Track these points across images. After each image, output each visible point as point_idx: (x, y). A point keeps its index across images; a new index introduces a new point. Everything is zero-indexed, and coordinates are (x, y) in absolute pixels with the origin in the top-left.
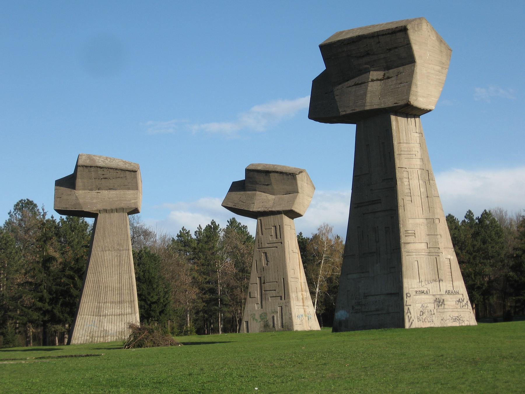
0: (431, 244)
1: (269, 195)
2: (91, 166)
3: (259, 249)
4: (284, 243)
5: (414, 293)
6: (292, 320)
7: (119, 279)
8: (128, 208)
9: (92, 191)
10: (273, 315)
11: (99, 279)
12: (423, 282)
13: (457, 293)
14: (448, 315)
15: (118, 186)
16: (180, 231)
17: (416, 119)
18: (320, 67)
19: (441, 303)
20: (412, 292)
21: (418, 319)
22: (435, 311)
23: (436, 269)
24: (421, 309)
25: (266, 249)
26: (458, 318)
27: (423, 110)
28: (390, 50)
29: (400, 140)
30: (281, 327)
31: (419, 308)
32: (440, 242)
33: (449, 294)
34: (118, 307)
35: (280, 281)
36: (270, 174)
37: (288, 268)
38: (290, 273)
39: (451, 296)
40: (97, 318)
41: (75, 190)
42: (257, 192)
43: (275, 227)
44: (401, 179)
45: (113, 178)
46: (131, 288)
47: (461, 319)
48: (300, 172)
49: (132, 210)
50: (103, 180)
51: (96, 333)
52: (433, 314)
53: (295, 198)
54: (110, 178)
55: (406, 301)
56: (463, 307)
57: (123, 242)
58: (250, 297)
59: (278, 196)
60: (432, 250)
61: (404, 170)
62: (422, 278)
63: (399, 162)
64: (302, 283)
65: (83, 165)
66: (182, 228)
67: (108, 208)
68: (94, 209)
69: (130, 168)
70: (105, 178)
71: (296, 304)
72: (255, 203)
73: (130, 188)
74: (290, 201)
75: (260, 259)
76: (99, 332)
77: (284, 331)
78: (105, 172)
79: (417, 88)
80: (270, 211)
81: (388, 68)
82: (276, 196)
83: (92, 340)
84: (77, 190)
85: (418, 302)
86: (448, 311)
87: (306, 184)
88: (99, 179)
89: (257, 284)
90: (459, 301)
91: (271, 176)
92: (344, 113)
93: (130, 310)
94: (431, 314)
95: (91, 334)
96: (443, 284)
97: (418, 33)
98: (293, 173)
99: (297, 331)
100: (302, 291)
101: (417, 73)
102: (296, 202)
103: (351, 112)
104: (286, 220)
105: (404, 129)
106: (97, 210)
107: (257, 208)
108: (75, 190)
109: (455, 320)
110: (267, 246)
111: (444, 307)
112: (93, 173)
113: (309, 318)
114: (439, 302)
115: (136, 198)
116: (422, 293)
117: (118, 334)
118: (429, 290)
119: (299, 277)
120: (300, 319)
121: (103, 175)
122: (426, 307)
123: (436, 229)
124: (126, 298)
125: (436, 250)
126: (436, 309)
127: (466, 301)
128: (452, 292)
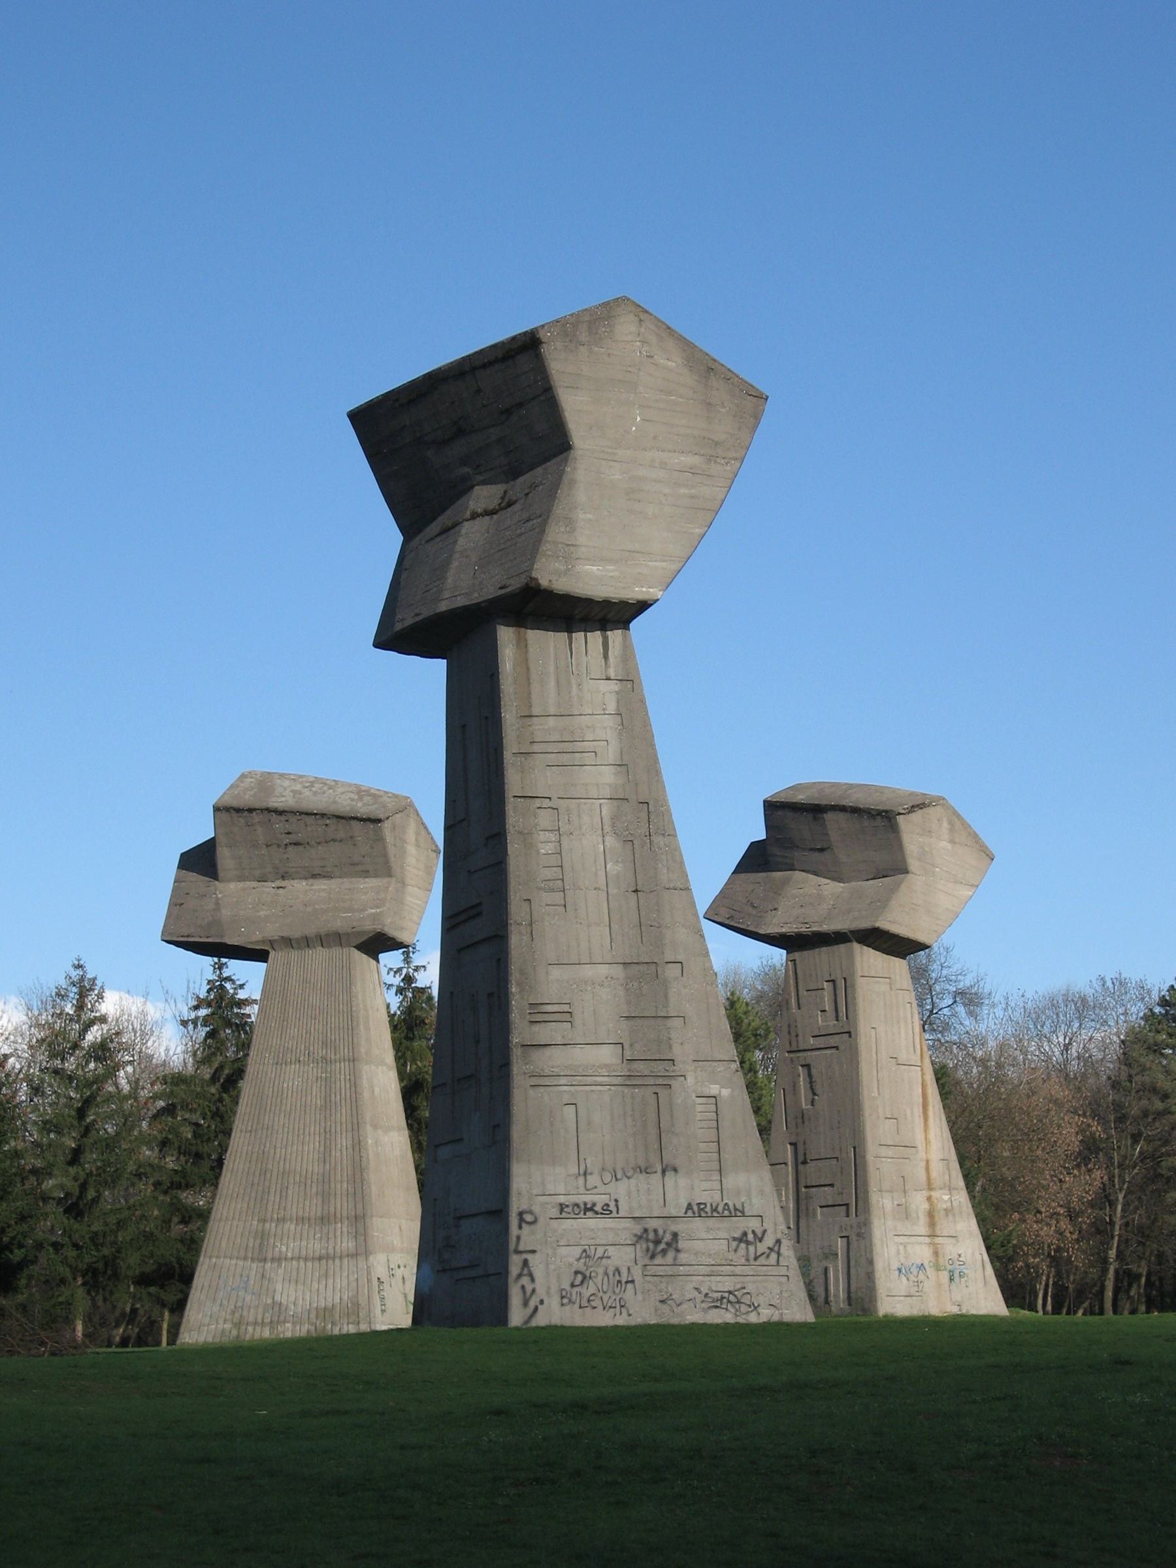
1: (829, 881)
2: (252, 807)
3: (792, 1055)
4: (857, 1035)
5: (555, 1212)
6: (874, 1282)
8: (353, 932)
9: (263, 883)
10: (825, 1263)
11: (266, 1149)
12: (591, 1174)
13: (739, 1212)
14: (690, 1286)
15: (336, 866)
17: (609, 633)
19: (662, 1246)
20: (544, 1207)
21: (562, 1297)
22: (637, 1273)
23: (653, 1132)
24: (580, 1266)
25: (809, 1053)
26: (732, 1298)
27: (607, 604)
28: (508, 412)
29: (531, 706)
30: (846, 1303)
31: (571, 1260)
32: (680, 1041)
33: (700, 1216)
36: (825, 815)
39: (711, 1222)
40: (254, 1266)
41: (217, 880)
42: (797, 872)
44: (526, 836)
45: (319, 843)
46: (358, 1176)
47: (746, 1299)
48: (913, 807)
49: (366, 937)
50: (290, 848)
51: (252, 1310)
52: (627, 1282)
53: (893, 890)
54: (308, 843)
55: (518, 1238)
56: (756, 1259)
59: (854, 883)
60: (641, 1067)
65: (228, 806)
67: (296, 934)
68: (254, 939)
72: (780, 908)
73: (368, 871)
74: (879, 901)
75: (794, 1086)
76: (260, 1310)
79: (573, 530)
81: (513, 473)
82: (847, 884)
83: (239, 1332)
84: (222, 881)
85: (568, 1241)
86: (691, 1273)
87: (945, 844)
89: (785, 1164)
90: (742, 1239)
91: (827, 823)
93: (352, 1245)
94: (619, 1282)
95: (237, 1315)
96: (676, 1182)
98: (886, 812)
100: (930, 1188)
101: (572, 482)
102: (893, 903)
104: (869, 960)
105: (552, 669)
106: (263, 942)
107: (779, 924)
108: (217, 882)
109: (719, 1302)
110: (812, 1045)
111: (675, 1259)
112: (260, 830)
113: (956, 1275)
114: (657, 1242)
116: (586, 1210)
117: (313, 1315)
118: (616, 1201)
120: (912, 1278)
121: (289, 833)
122: (602, 1258)
125: (659, 1068)
126: (640, 1266)
127: (774, 1241)
128: (715, 1210)
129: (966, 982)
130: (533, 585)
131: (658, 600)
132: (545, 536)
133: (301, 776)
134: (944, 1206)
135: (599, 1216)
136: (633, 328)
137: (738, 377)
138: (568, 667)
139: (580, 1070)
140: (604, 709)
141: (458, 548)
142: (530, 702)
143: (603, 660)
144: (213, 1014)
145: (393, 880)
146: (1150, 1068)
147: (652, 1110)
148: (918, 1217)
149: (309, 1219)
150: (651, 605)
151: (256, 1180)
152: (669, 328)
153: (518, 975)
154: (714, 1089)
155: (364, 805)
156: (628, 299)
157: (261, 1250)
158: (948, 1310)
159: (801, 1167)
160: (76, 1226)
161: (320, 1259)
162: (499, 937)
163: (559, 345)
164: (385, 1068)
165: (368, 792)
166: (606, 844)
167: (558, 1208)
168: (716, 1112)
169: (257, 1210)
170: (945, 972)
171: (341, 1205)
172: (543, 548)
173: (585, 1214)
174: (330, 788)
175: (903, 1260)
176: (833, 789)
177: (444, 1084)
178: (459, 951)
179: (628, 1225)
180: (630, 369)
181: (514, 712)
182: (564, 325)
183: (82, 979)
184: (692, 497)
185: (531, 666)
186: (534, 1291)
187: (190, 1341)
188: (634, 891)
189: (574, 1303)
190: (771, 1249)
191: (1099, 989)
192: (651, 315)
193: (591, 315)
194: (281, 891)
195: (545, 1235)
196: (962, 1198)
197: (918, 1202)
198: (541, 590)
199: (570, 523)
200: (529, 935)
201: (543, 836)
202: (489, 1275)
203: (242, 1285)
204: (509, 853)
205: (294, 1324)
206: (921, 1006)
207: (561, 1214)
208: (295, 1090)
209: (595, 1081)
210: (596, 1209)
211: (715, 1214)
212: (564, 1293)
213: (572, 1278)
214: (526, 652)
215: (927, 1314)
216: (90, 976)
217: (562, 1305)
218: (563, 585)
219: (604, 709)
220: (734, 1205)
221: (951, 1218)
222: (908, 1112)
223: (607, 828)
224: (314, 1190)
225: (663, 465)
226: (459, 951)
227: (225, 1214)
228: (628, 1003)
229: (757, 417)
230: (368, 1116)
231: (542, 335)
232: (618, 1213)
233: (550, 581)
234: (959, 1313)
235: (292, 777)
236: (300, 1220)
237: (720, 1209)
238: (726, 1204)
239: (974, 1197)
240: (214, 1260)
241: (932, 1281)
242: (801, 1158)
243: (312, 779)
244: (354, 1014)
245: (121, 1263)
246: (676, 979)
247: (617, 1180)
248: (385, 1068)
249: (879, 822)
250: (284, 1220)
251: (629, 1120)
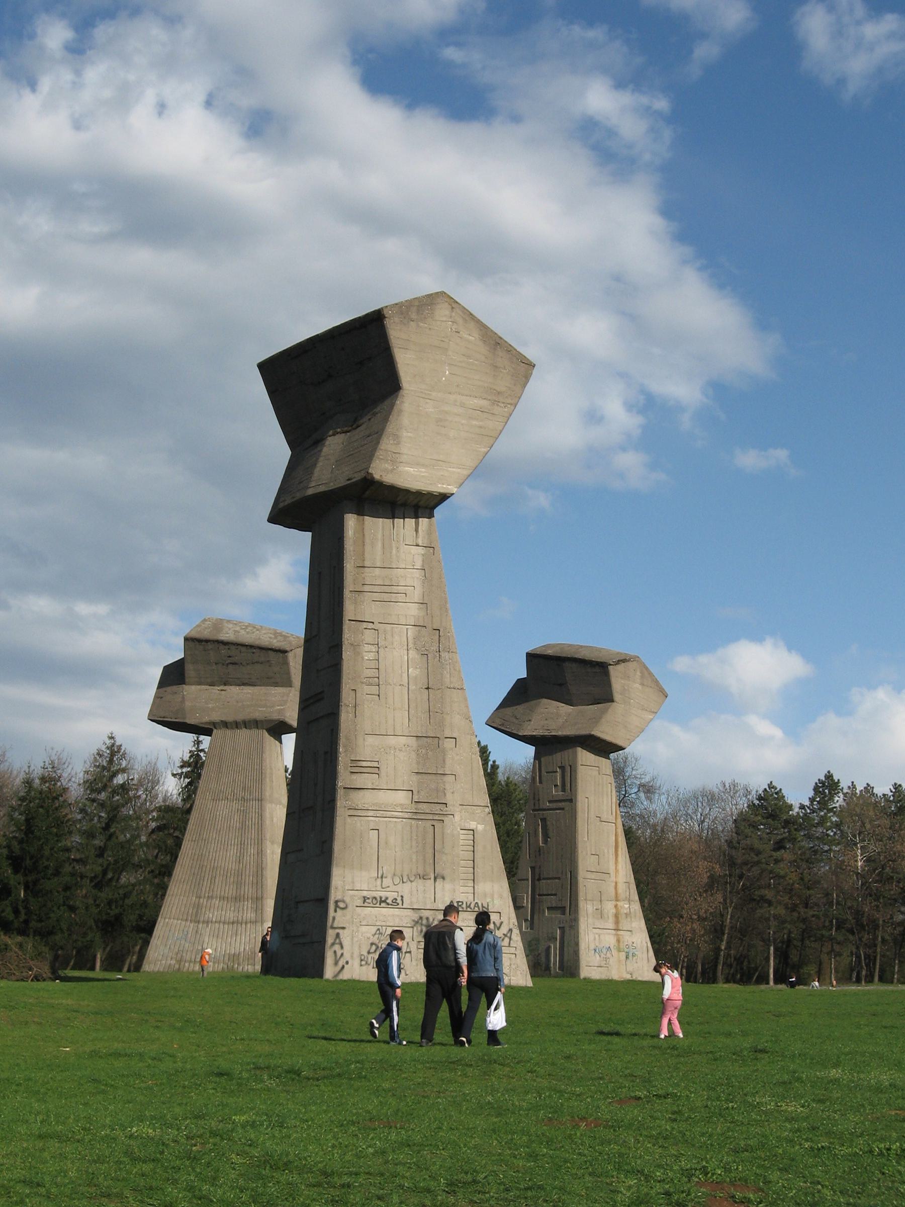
0: (422, 793)
5: (359, 902)
6: (578, 957)
7: (238, 854)
11: (204, 853)
12: (386, 877)
16: (765, 789)
20: (353, 899)
23: (431, 851)
29: (364, 560)
31: (369, 935)
32: (451, 791)
34: (232, 908)
38: (586, 862)
40: (192, 925)
44: (355, 646)
48: (618, 661)
50: (230, 666)
51: (188, 953)
52: (406, 953)
55: (334, 918)
57: (252, 784)
61: (365, 627)
62: (387, 869)
63: (355, 608)
64: (618, 884)
66: (768, 784)
67: (230, 718)
70: (233, 664)
71: (594, 925)
72: (533, 720)
74: (594, 718)
76: (194, 954)
77: (563, 976)
79: (399, 443)
85: (368, 922)
87: (637, 685)
88: (223, 664)
93: (253, 915)
95: (179, 955)
97: (418, 325)
99: (587, 981)
101: (400, 411)
104: (584, 757)
105: (380, 536)
106: (209, 723)
113: (630, 955)
116: (381, 902)
117: (226, 958)
118: (402, 897)
120: (602, 955)
121: (230, 657)
123: (444, 761)
124: (249, 891)
125: (437, 808)
126: (415, 941)
127: (508, 929)
129: (646, 779)
130: (369, 478)
131: (453, 494)
132: (379, 446)
133: (240, 622)
134: (625, 912)
135: (390, 906)
136: (447, 312)
137: (516, 350)
138: (391, 535)
139: (383, 806)
140: (413, 566)
141: (323, 454)
142: (363, 557)
143: (415, 533)
144: (193, 771)
145: (293, 688)
146: (751, 837)
147: (431, 836)
148: (608, 917)
149: (227, 898)
150: (449, 497)
151: (196, 873)
152: (471, 314)
153: (344, 740)
154: (473, 825)
155: (278, 641)
156: (445, 293)
157: (196, 915)
158: (624, 977)
159: (537, 883)
160: (99, 894)
161: (233, 923)
162: (333, 715)
163: (396, 319)
164: (281, 806)
165: (281, 634)
166: (410, 655)
167: (363, 899)
168: (473, 841)
169: (195, 891)
170: (634, 772)
171: (249, 891)
172: (377, 454)
173: (380, 904)
174: (258, 630)
175: (597, 944)
176: (570, 648)
177: (294, 812)
178: (309, 723)
179: (409, 914)
180: (443, 339)
181: (352, 563)
182: (401, 307)
183: (113, 745)
184: (481, 427)
185: (366, 533)
186: (342, 954)
187: (149, 970)
188: (426, 688)
189: (369, 965)
190: (505, 935)
191: (722, 789)
192: (460, 304)
193: (420, 302)
194: (223, 692)
195: (352, 917)
196: (636, 907)
197: (609, 908)
198: (375, 482)
199: (397, 437)
200: (354, 714)
201: (367, 648)
202: (313, 943)
203: (184, 937)
204: (343, 657)
205: (214, 963)
206: (619, 791)
207: (364, 903)
208: (224, 816)
209: (386, 814)
210: (388, 901)
211: (469, 909)
212: (363, 958)
213: (369, 947)
214: (363, 524)
215: (610, 978)
216: (118, 743)
217: (361, 965)
218: (389, 479)
219: (413, 566)
220: (482, 904)
221: (629, 919)
222: (606, 851)
223: (411, 645)
224: (232, 880)
225: (462, 405)
226: (309, 723)
227: (175, 893)
228: (418, 763)
229: (527, 377)
230: (268, 836)
231: (385, 312)
232: (402, 905)
233: (381, 476)
234: (631, 979)
235: (235, 622)
236: (222, 898)
237: (472, 906)
238: (477, 903)
239: (644, 906)
240: (167, 920)
241: (616, 958)
242: (537, 877)
243: (246, 624)
244: (263, 771)
245: (125, 917)
246: (452, 749)
247: (403, 882)
248: (281, 806)
249: (597, 670)
250: (212, 897)
251: (414, 843)
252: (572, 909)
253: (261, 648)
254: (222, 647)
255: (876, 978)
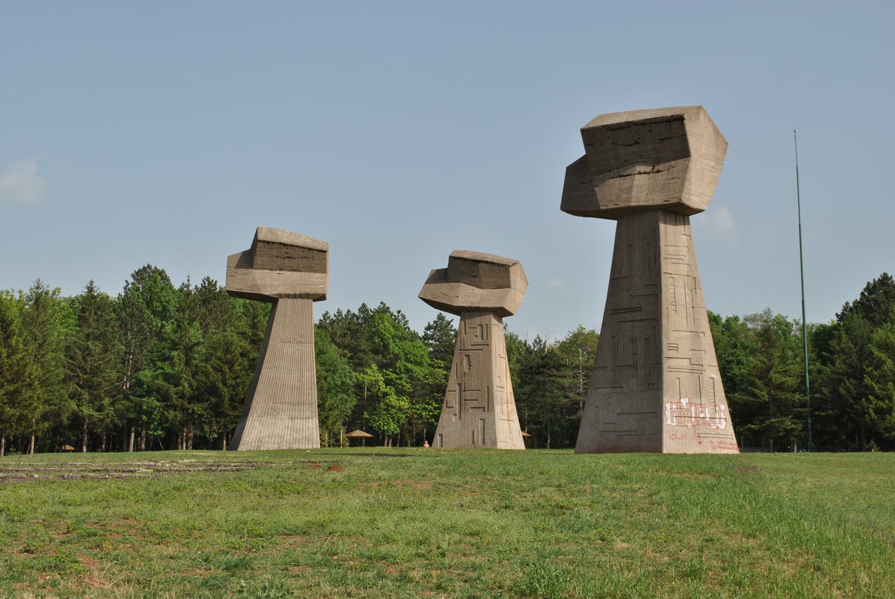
18: (579, 151)
27: (696, 209)
34: (297, 410)
35: (483, 389)
37: (494, 374)
38: (496, 382)
43: (481, 326)
58: (447, 407)
60: (696, 367)
67: (291, 292)
69: (319, 247)
78: (290, 250)
80: (476, 307)
88: (281, 258)
92: (605, 208)
103: (614, 207)
115: (324, 283)
119: (505, 387)
194: (280, 275)
249: (501, 268)
252: (490, 408)
253: (310, 249)
254: (282, 247)
255: (131, 448)
